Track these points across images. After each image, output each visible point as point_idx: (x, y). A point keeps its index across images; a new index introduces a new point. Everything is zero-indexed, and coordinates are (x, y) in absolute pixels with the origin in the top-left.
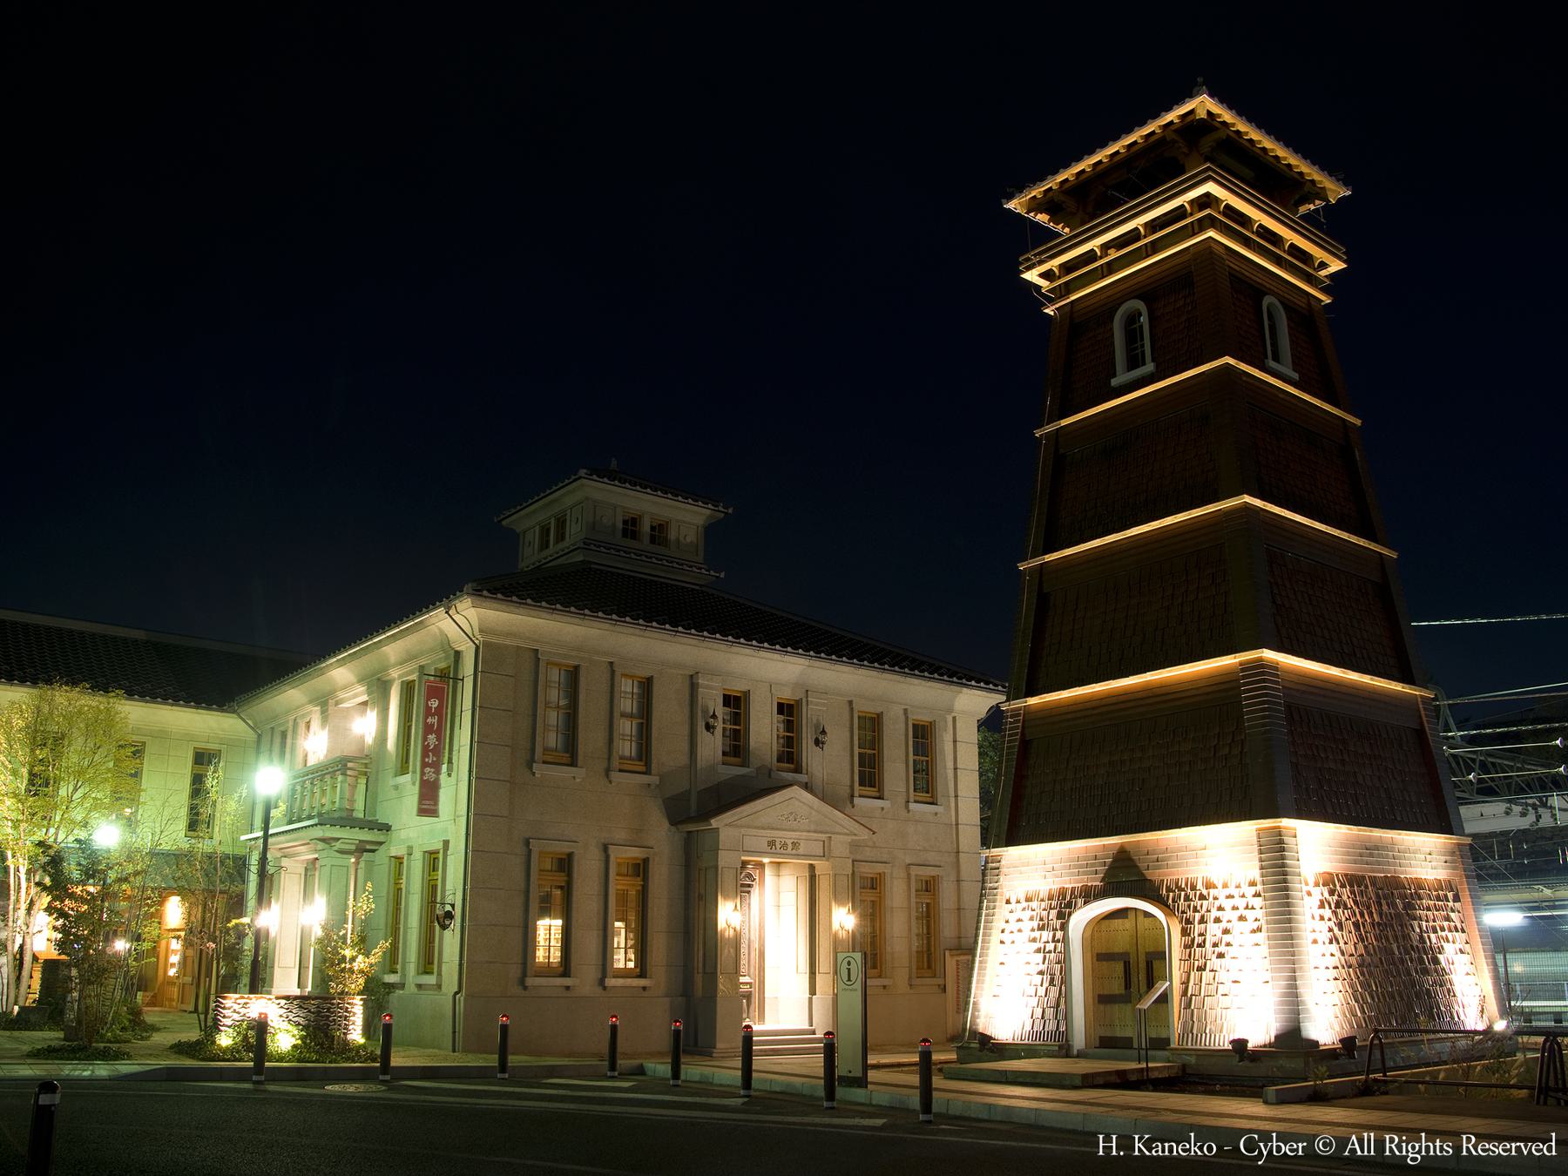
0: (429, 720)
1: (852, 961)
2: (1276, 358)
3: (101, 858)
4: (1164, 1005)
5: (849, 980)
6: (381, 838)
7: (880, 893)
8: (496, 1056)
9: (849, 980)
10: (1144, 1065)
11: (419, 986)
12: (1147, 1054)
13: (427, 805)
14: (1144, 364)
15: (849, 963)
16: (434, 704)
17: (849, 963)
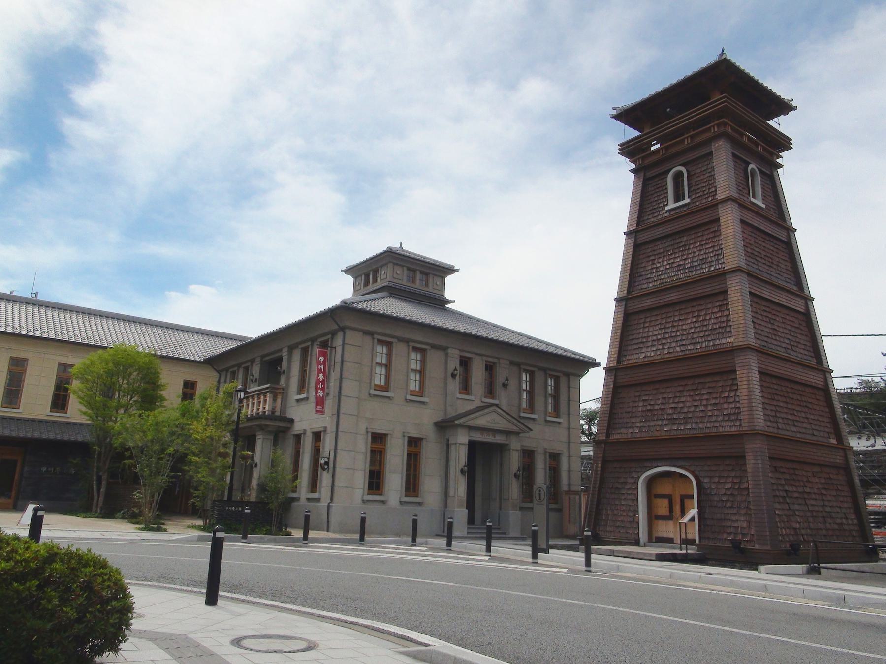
0: (320, 367)
1: (542, 490)
2: (754, 197)
3: (191, 432)
4: (693, 522)
5: (540, 499)
6: (289, 426)
7: (423, 393)
8: (359, 535)
9: (540, 499)
10: (685, 552)
11: (308, 499)
12: (338, 325)
13: (320, 408)
14: (684, 199)
15: (540, 491)
16: (322, 359)
17: (540, 491)
